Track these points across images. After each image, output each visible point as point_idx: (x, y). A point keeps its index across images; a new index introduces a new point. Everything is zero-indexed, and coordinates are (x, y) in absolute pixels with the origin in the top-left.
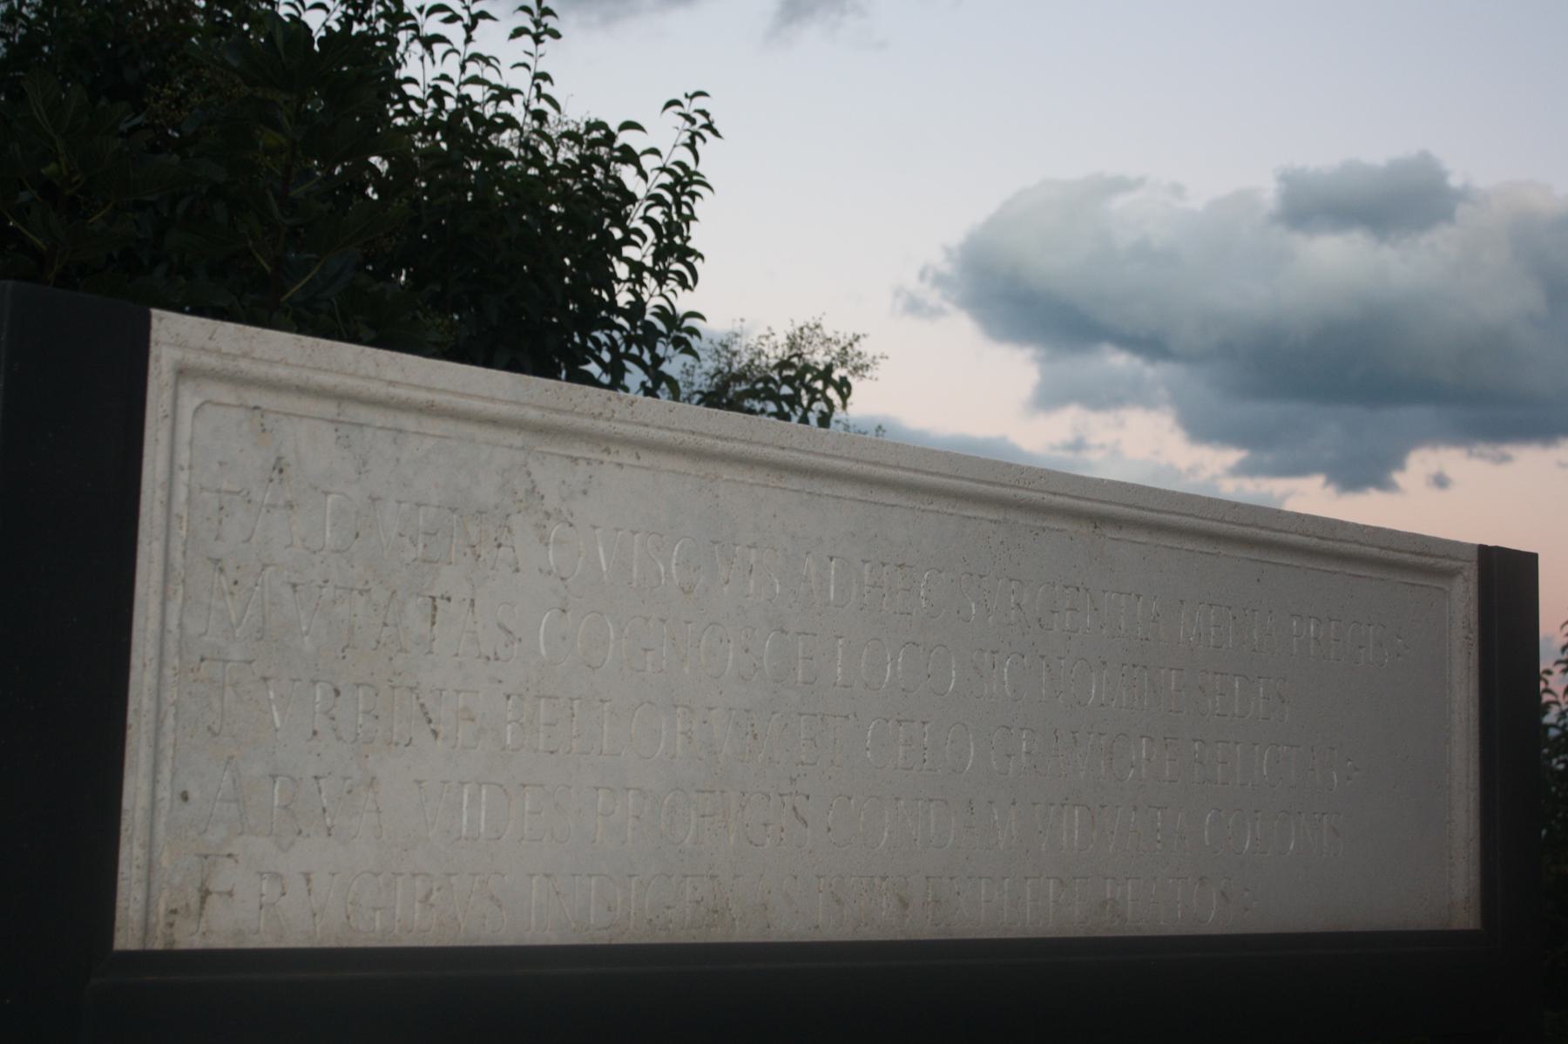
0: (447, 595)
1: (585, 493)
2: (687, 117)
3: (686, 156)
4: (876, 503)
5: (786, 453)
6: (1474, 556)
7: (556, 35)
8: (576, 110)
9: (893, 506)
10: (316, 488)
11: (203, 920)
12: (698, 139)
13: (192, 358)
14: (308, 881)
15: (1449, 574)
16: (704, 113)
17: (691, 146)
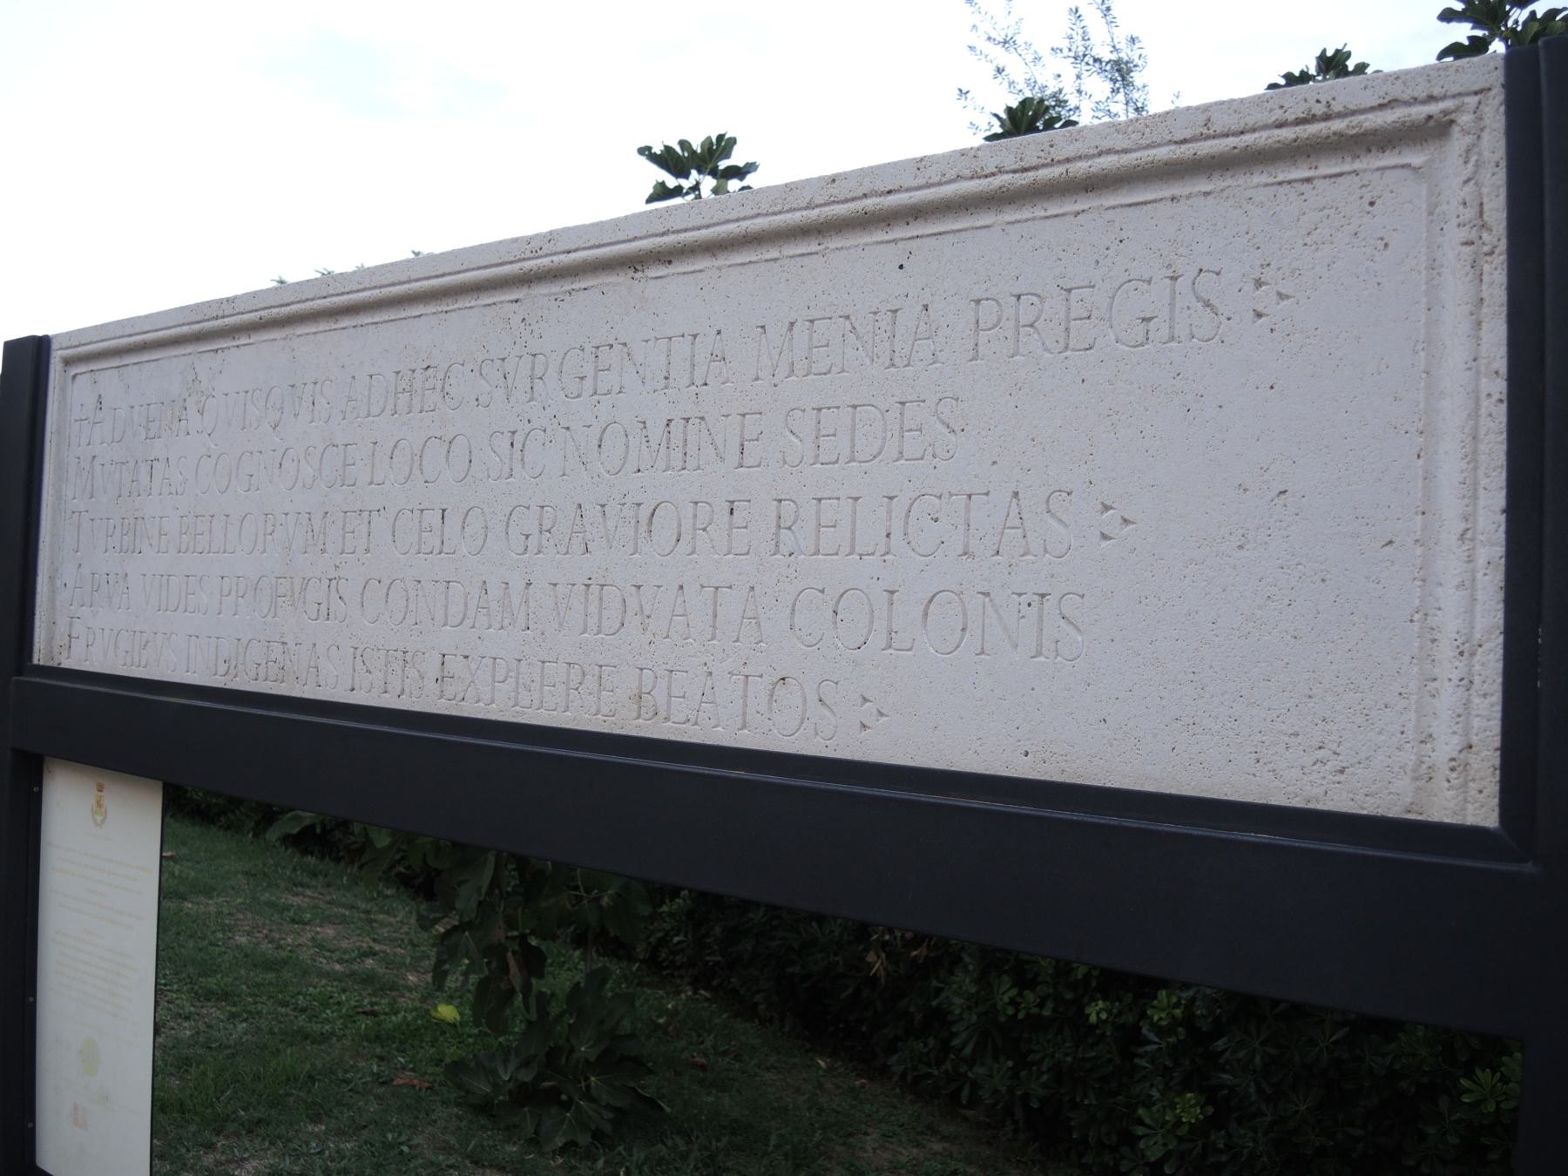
1: (221, 372)
4: (405, 319)
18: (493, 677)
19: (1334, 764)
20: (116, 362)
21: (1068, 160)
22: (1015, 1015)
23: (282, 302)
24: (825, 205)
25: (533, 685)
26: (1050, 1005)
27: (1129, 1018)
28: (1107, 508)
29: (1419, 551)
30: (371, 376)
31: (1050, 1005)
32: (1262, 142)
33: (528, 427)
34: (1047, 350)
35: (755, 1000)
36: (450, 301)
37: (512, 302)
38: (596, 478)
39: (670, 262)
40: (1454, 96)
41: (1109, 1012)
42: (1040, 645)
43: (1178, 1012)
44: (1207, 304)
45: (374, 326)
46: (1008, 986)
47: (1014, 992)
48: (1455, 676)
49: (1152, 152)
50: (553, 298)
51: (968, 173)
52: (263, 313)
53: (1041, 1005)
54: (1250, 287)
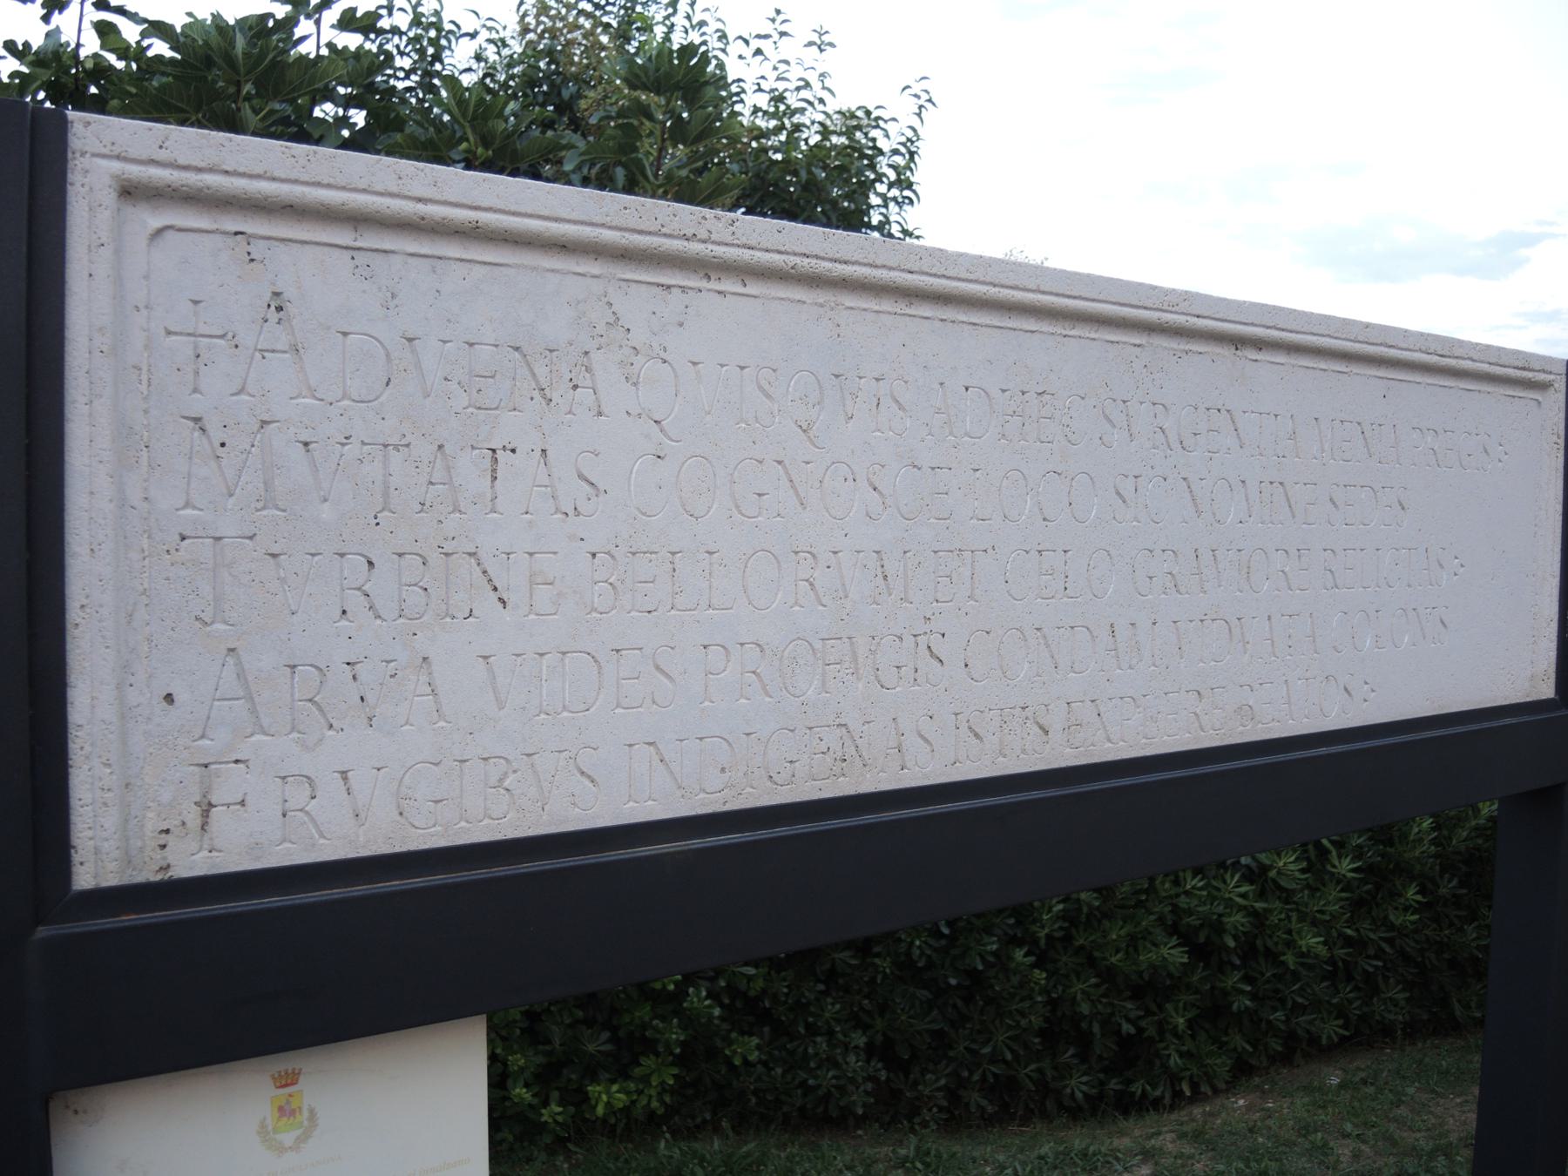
0: (510, 446)
1: (681, 325)
2: (916, 96)
3: (916, 122)
4: (1015, 330)
5: (914, 277)
6: (1565, 363)
7: (832, 45)
8: (846, 98)
9: (1033, 332)
10: (329, 328)
11: (206, 837)
12: (923, 109)
13: (135, 171)
14: (345, 779)
15: (1543, 386)
16: (926, 91)
17: (919, 115)
20: (344, 237)
23: (837, 256)
35: (1170, 923)
36: (1066, 325)
37: (1135, 345)
45: (970, 327)
50: (1172, 353)
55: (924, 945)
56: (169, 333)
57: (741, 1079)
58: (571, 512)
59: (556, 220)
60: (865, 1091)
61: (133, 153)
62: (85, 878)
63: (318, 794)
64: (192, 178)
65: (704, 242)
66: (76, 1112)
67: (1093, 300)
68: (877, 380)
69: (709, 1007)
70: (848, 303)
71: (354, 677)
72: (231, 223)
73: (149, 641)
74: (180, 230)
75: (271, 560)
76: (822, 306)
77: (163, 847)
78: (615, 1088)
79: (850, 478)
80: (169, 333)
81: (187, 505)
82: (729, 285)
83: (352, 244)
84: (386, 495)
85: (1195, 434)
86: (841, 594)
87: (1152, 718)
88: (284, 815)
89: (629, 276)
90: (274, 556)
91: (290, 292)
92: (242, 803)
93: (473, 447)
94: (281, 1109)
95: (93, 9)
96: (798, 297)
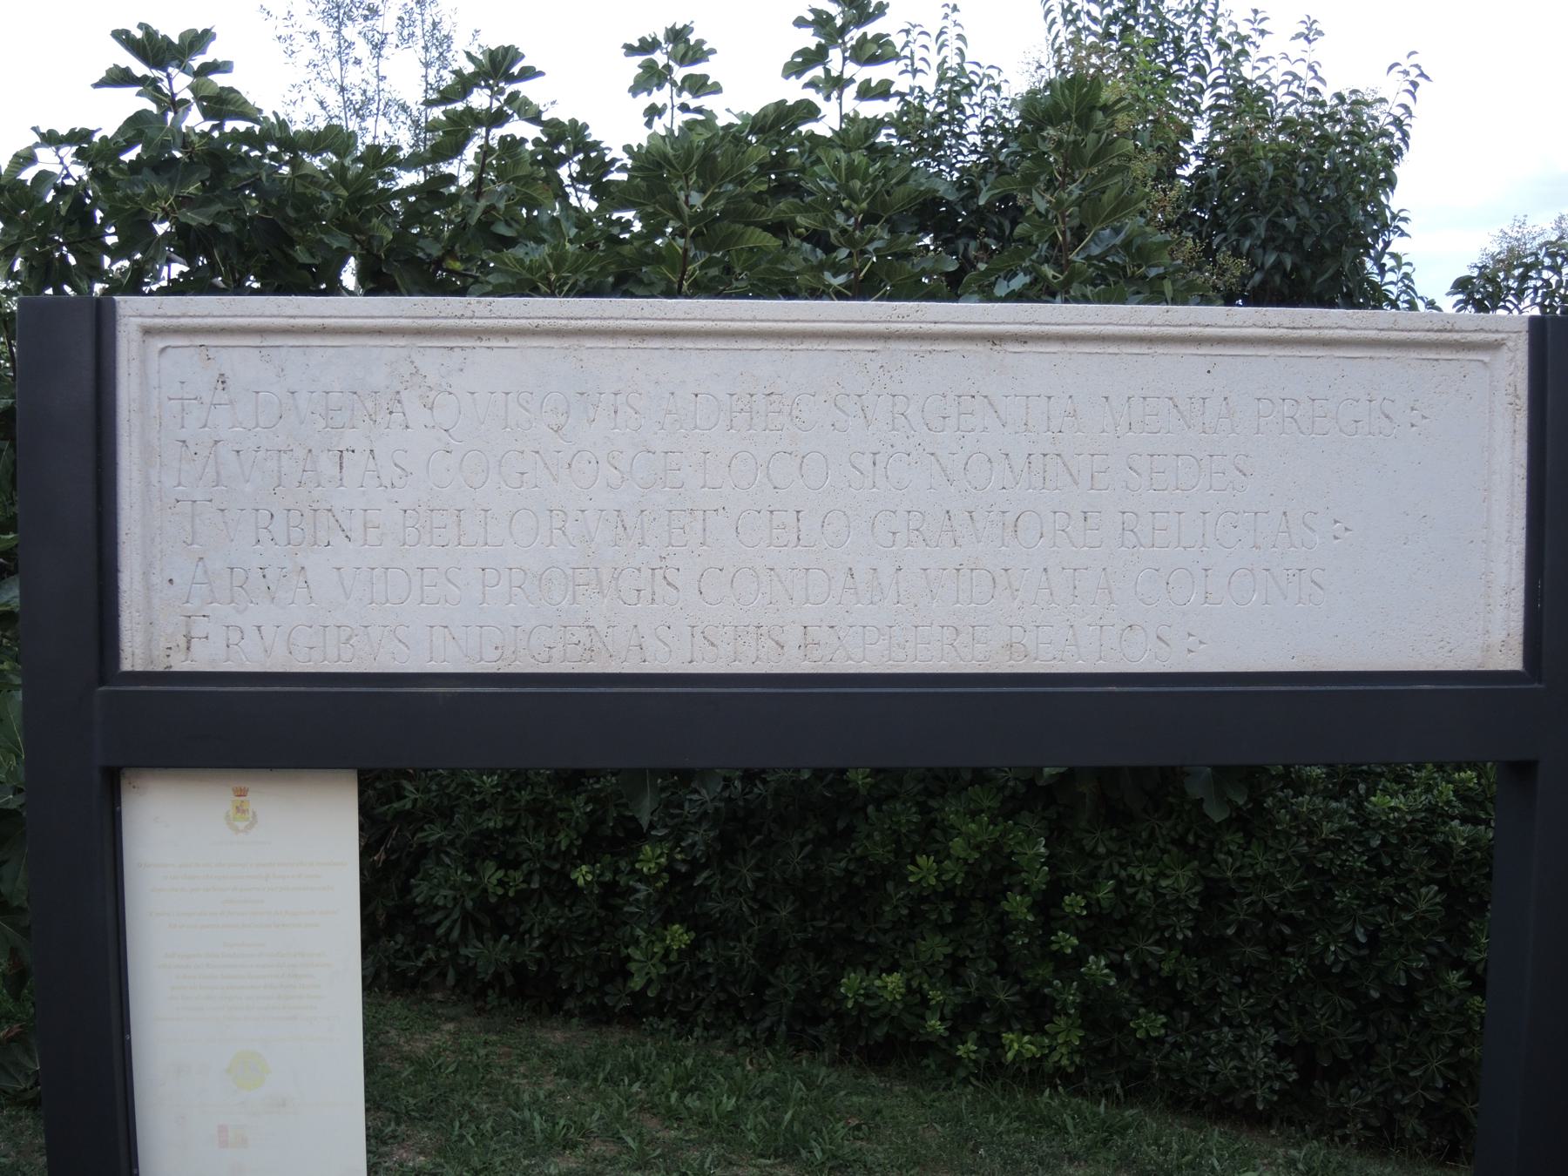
5: (638, 322)
13: (148, 322)
15: (1495, 346)
16: (1417, 66)
18: (864, 639)
19: (1448, 648)
20: (256, 341)
21: (1320, 328)
22: (506, 894)
23: (571, 315)
24: (1163, 325)
25: (908, 644)
26: (536, 878)
27: (608, 877)
28: (1336, 522)
29: (1484, 546)
30: (696, 395)
31: (536, 878)
32: (1422, 338)
33: (891, 451)
34: (1302, 433)
38: (963, 492)
39: (1025, 342)
40: (1507, 332)
41: (593, 873)
42: (1300, 598)
43: (663, 860)
44: (1387, 417)
46: (493, 870)
47: (500, 874)
48: (1504, 603)
49: (1366, 332)
51: (1260, 324)
52: (540, 322)
53: (527, 880)
54: (1409, 410)
55: (1339, 951)
56: (170, 399)
57: (1147, 1053)
58: (389, 486)
59: (372, 317)
60: (1271, 1088)
61: (147, 313)
62: (126, 666)
63: (245, 636)
64: (174, 321)
65: (471, 318)
66: (134, 787)
67: (814, 321)
68: (616, 394)
69: (1107, 975)
70: (589, 345)
71: (264, 576)
72: (198, 341)
73: (161, 552)
74: (174, 347)
75: (220, 513)
76: (566, 348)
77: (168, 656)
78: (1026, 1038)
79: (594, 461)
80: (170, 399)
81: (179, 484)
82: (495, 343)
83: (258, 344)
84: (280, 478)
85: (944, 418)
86: (587, 538)
87: (898, 645)
88: (228, 646)
89: (424, 344)
90: (222, 510)
91: (228, 373)
92: (207, 637)
93: (329, 450)
94: (237, 808)
95: (680, 112)
96: (547, 344)
